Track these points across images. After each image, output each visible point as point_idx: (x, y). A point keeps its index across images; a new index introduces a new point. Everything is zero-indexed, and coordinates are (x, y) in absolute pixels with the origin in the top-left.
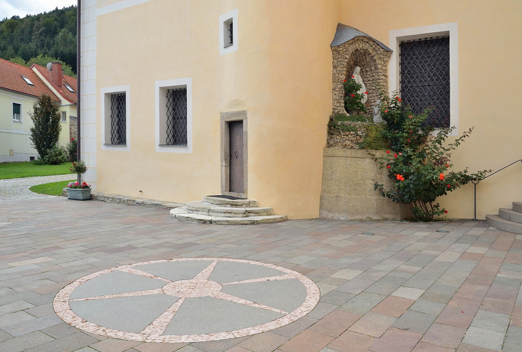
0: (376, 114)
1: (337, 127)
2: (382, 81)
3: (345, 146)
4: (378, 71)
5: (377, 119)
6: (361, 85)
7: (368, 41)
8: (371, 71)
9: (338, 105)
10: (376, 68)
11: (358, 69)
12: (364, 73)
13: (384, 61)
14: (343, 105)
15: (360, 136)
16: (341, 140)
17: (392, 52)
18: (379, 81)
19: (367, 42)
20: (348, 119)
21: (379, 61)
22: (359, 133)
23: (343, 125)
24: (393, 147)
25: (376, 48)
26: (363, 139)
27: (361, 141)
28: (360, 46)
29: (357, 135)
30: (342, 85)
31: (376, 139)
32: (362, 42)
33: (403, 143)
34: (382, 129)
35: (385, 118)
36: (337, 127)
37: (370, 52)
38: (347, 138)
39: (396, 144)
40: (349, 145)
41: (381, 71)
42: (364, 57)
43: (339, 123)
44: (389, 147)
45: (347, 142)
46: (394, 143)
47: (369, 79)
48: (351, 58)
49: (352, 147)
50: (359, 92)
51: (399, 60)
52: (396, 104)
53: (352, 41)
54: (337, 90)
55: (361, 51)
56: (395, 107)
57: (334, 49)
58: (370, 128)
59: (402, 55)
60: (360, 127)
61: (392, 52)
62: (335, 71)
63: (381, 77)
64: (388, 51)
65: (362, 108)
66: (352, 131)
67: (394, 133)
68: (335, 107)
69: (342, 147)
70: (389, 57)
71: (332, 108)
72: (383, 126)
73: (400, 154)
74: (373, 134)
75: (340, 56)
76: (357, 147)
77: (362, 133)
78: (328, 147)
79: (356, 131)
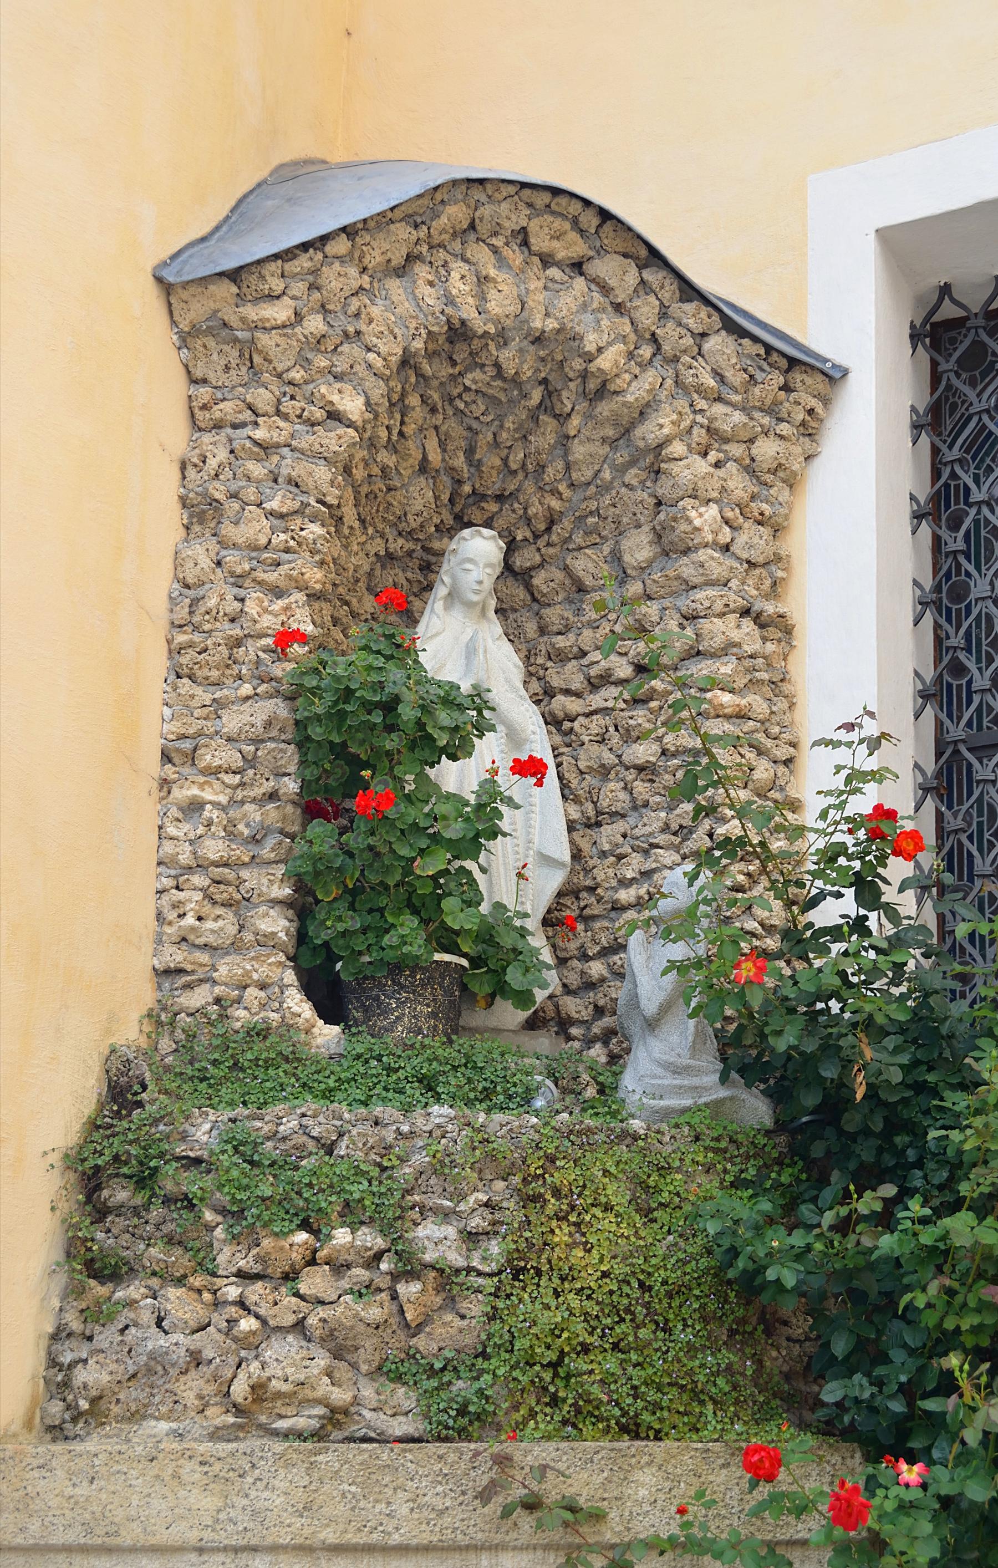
0: (652, 1024)
1: (173, 1180)
2: (726, 668)
3: (252, 1413)
4: (686, 568)
5: (668, 1072)
6: (480, 700)
7: (579, 248)
8: (623, 577)
9: (221, 926)
10: (671, 545)
11: (478, 552)
12: (553, 615)
13: (750, 468)
14: (278, 924)
15: (447, 1280)
16: (209, 1344)
17: (833, 377)
18: (700, 669)
19: (578, 266)
20: (321, 1083)
21: (702, 466)
22: (436, 1239)
23: (243, 1148)
24: (831, 1392)
25: (668, 332)
26: (475, 1307)
27: (451, 1332)
28: (499, 292)
29: (410, 1268)
30: (281, 709)
31: (636, 1305)
32: (515, 256)
33: (945, 1341)
34: (709, 1183)
35: (741, 1054)
36: (173, 1180)
37: (605, 362)
38: (285, 1309)
39: (868, 1356)
40: (297, 1397)
41: (718, 565)
42: (545, 437)
43: (204, 1132)
44: (790, 1394)
45: (285, 1361)
46: (840, 1347)
47: (600, 662)
48: (384, 434)
49: (337, 1416)
50: (457, 778)
51: (908, 475)
52: (868, 891)
53: (403, 232)
54: (218, 755)
55: (508, 357)
56: (859, 925)
57: (196, 310)
58: (565, 1175)
59: (937, 419)
60: (441, 1166)
61: (833, 377)
62: (201, 554)
63: (721, 629)
64: (797, 375)
65: (489, 963)
66: (351, 1214)
67: (844, 1226)
68: (175, 956)
69: (220, 1417)
70: (810, 429)
71: (142, 961)
72: (723, 1144)
73: (911, 1473)
74: (606, 1246)
75: (263, 397)
76: (397, 1409)
77: (471, 1238)
78: (56, 1432)
79: (393, 1220)
